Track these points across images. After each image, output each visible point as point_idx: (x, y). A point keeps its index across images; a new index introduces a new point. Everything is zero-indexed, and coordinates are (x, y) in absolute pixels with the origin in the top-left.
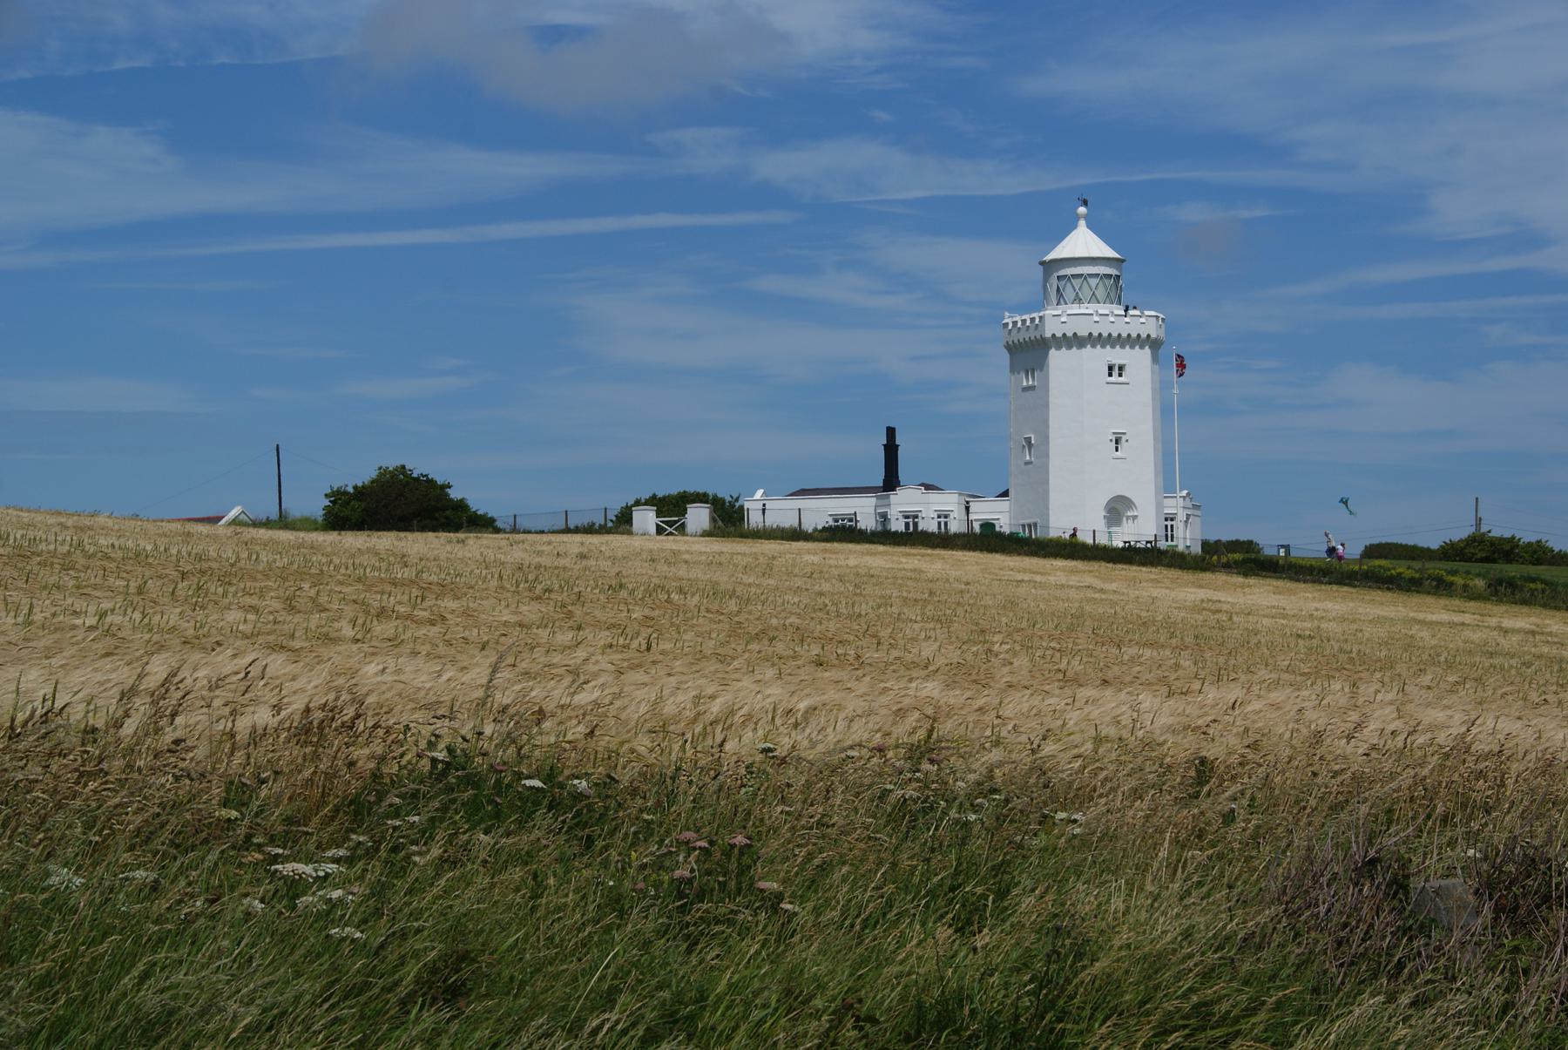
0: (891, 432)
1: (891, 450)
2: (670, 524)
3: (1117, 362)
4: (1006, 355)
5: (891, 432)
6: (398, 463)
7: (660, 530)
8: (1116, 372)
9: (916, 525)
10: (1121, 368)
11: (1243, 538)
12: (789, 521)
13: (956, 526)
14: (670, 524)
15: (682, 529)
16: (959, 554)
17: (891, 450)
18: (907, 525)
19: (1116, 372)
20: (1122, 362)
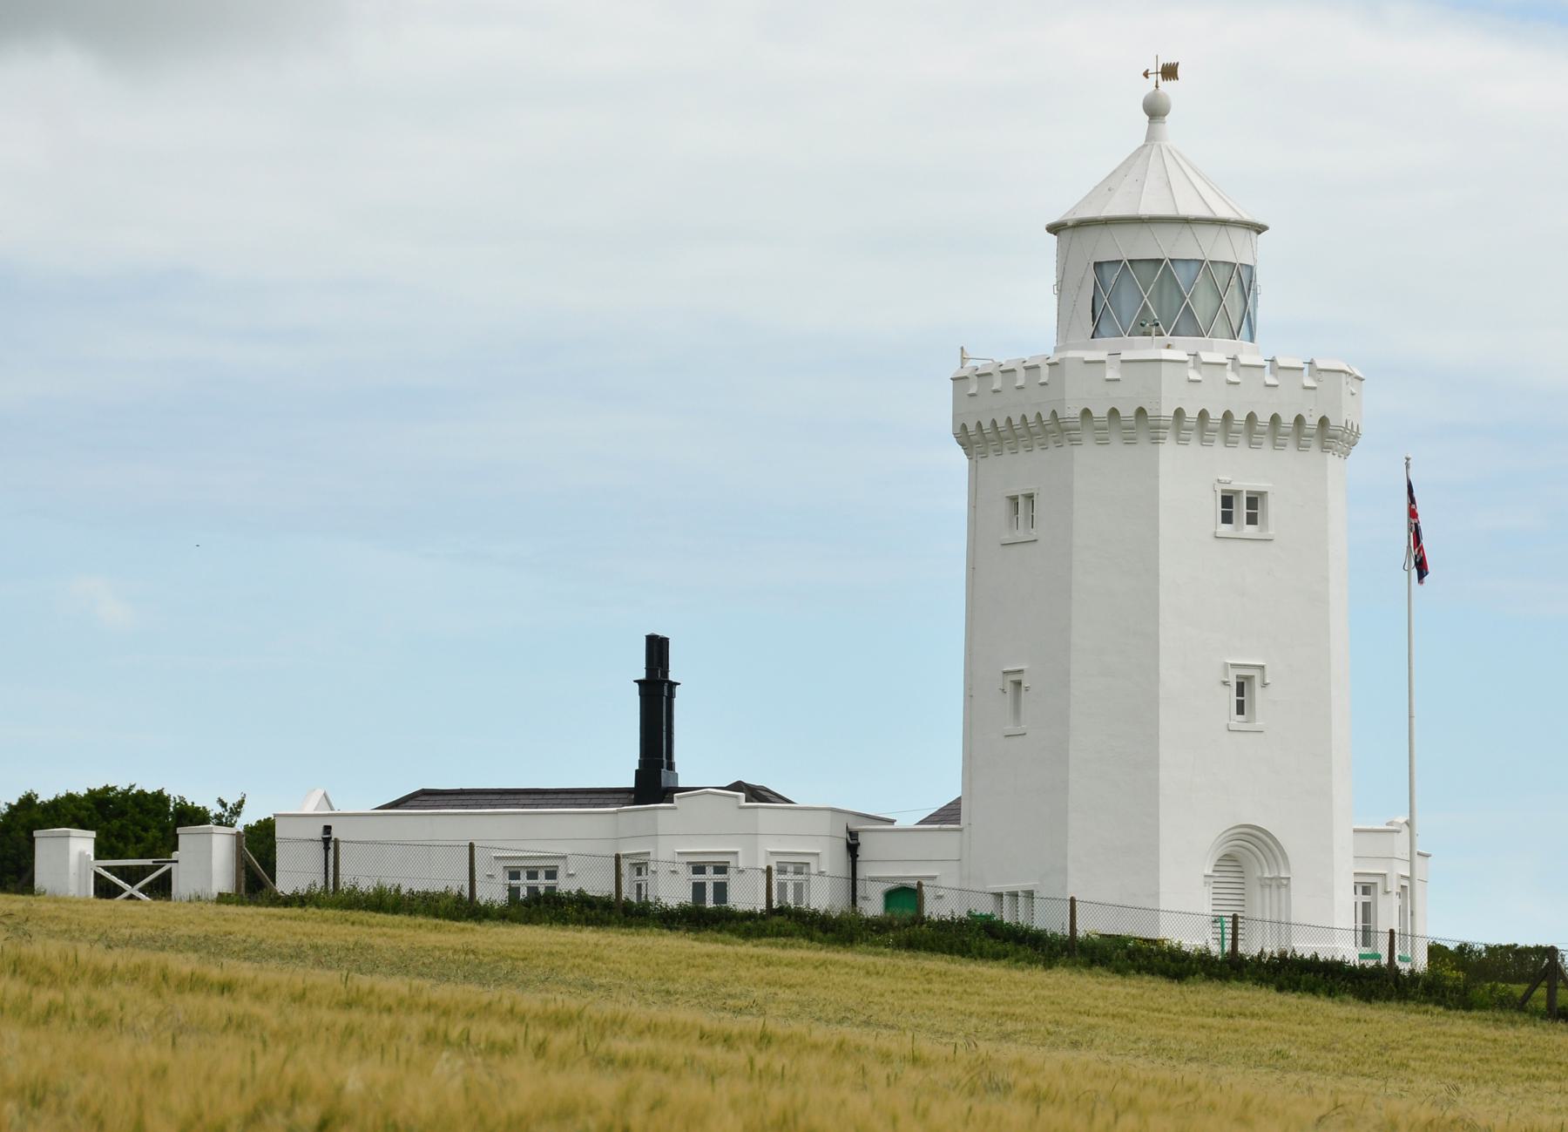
0: (657, 649)
1: (656, 694)
2: (131, 875)
3: (1245, 484)
4: (958, 458)
5: (657, 649)
6: (21, 794)
7: (105, 889)
8: (1241, 510)
9: (721, 890)
10: (1253, 501)
11: (1526, 938)
12: (447, 878)
13: (822, 897)
14: (131, 875)
15: (162, 888)
16: (883, 960)
17: (656, 694)
18: (699, 889)
19: (1241, 510)
20: (1028, 885)
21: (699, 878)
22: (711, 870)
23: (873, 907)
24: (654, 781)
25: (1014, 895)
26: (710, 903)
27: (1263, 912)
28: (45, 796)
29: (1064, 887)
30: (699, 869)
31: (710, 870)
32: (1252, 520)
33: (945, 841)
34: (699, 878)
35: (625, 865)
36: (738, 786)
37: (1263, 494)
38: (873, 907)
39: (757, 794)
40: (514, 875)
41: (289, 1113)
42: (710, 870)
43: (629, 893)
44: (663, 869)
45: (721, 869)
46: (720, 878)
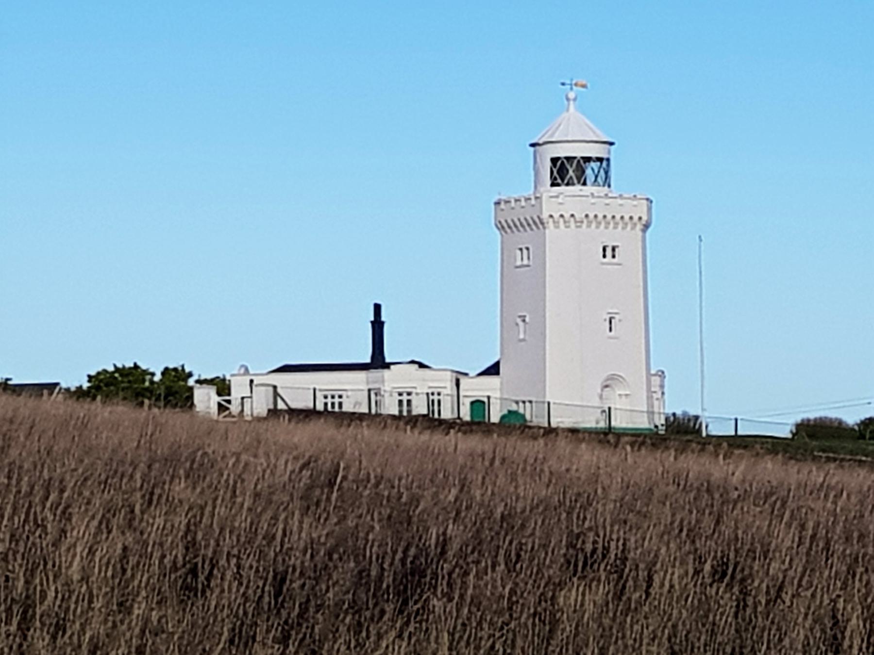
0: (377, 308)
1: (378, 326)
5: (377, 308)
8: (609, 252)
9: (340, 404)
17: (378, 326)
18: (326, 404)
19: (609, 252)
21: (401, 398)
24: (378, 361)
25: (524, 402)
26: (337, 409)
28: (372, 319)
29: (544, 396)
30: (400, 394)
31: (405, 395)
32: (614, 256)
34: (401, 398)
35: (318, 394)
36: (413, 362)
37: (618, 246)
39: (422, 366)
40: (400, 394)
41: (340, 554)
42: (405, 395)
44: (387, 395)
45: (409, 394)
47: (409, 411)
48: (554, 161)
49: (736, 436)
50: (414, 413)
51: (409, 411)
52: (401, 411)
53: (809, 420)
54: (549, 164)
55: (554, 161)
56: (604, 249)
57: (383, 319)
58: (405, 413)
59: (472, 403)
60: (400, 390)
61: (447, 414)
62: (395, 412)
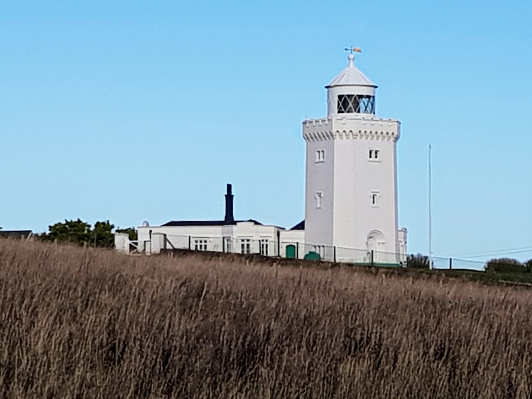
0: (229, 187)
1: (229, 198)
5: (229, 187)
8: (373, 154)
9: (205, 246)
17: (229, 198)
18: (196, 246)
19: (373, 154)
21: (243, 243)
22: (246, 244)
23: (283, 254)
24: (229, 220)
25: (319, 247)
26: (203, 249)
27: (403, 252)
28: (226, 194)
29: (332, 243)
30: (243, 241)
31: (246, 241)
32: (376, 157)
33: (300, 233)
34: (243, 243)
35: (192, 239)
36: (251, 221)
37: (379, 151)
38: (283, 254)
39: (256, 223)
42: (246, 241)
43: (193, 248)
44: (234, 241)
45: (248, 240)
46: (248, 243)
47: (248, 251)
48: (340, 97)
49: (451, 270)
50: (251, 252)
51: (248, 251)
52: (243, 251)
53: (496, 260)
54: (337, 99)
55: (340, 97)
56: (370, 153)
57: (233, 194)
58: (245, 253)
59: (287, 247)
60: (243, 238)
61: (271, 253)
62: (239, 251)
